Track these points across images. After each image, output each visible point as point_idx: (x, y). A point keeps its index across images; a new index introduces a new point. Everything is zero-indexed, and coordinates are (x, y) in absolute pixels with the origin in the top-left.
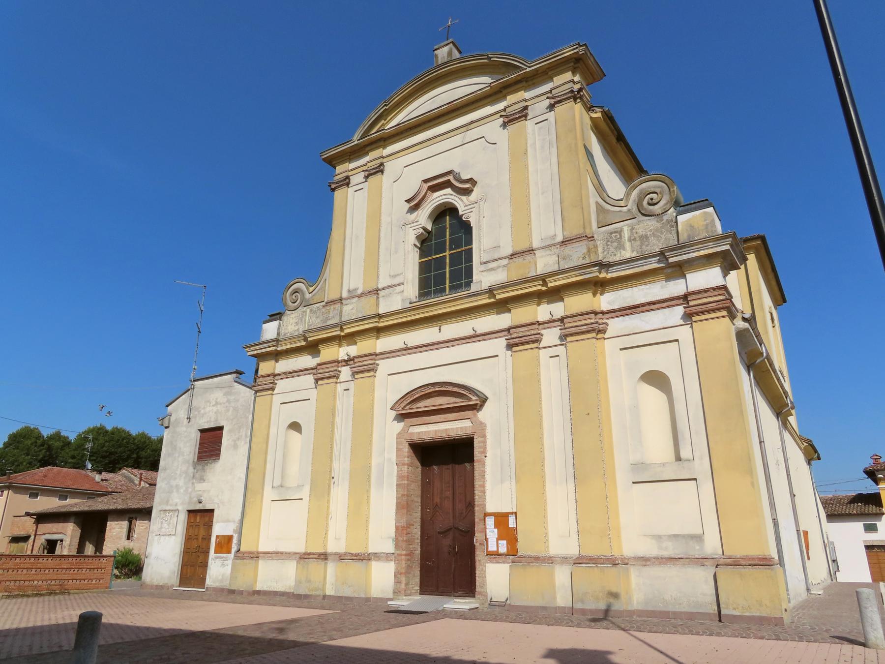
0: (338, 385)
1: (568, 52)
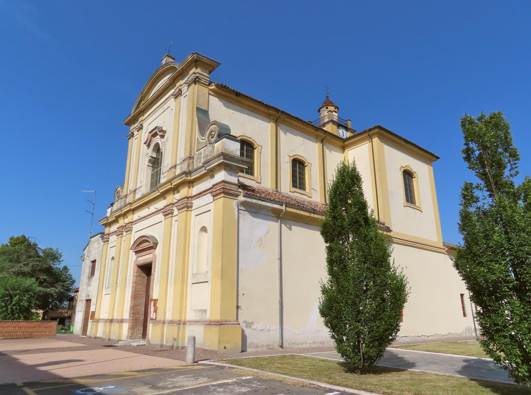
0: (173, 218)
1: (190, 58)
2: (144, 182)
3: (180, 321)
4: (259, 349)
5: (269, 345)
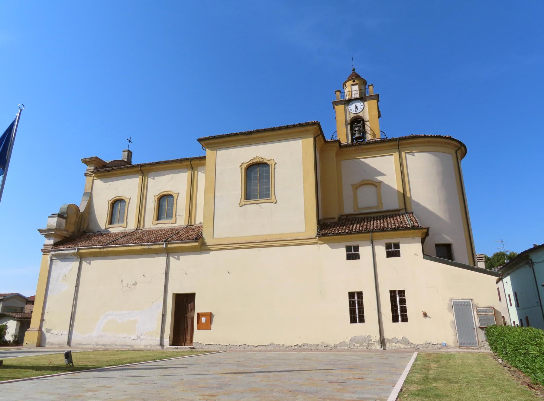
4: (53, 346)
5: (61, 344)
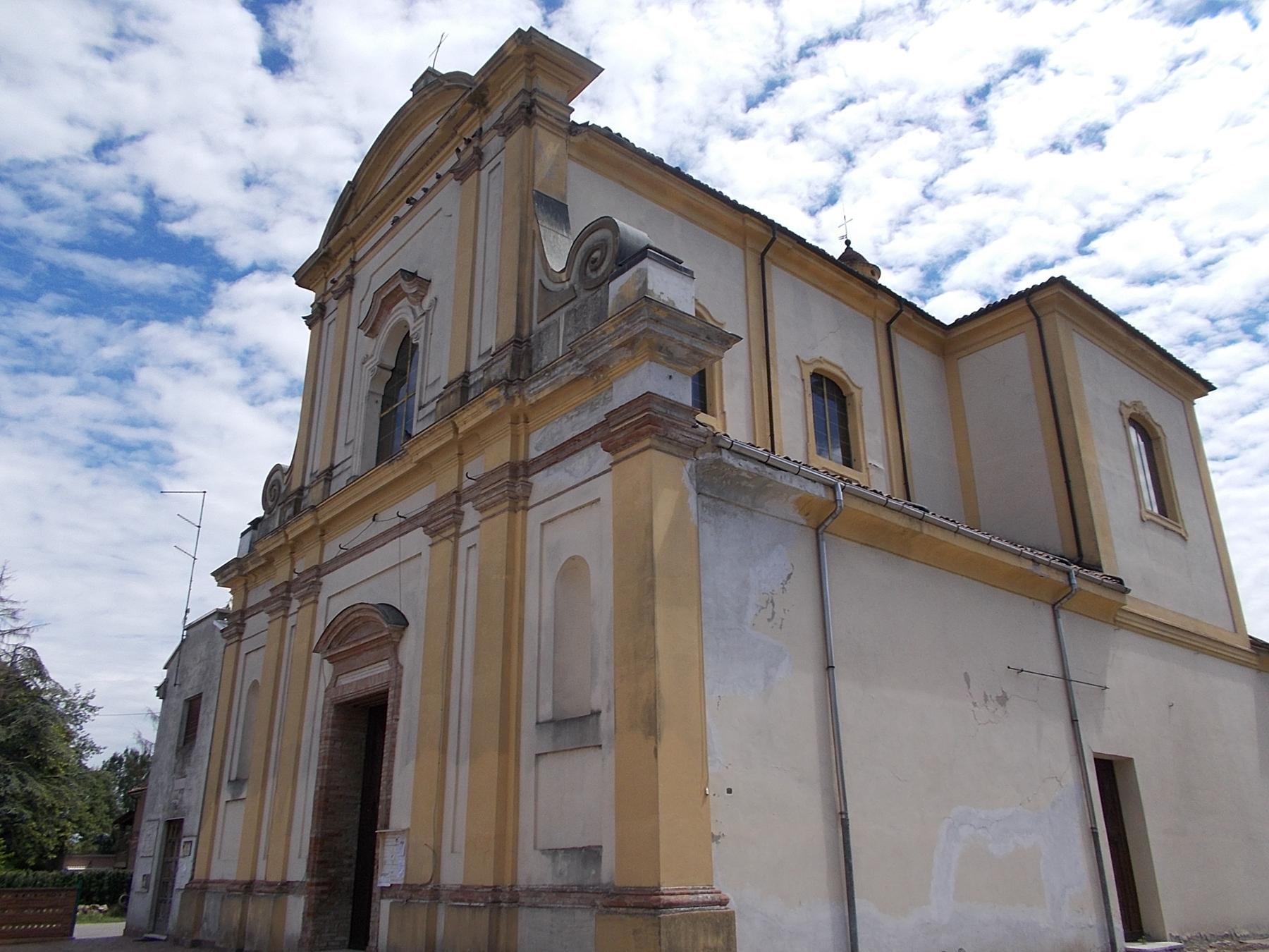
2: (359, 443)
3: (495, 889)
